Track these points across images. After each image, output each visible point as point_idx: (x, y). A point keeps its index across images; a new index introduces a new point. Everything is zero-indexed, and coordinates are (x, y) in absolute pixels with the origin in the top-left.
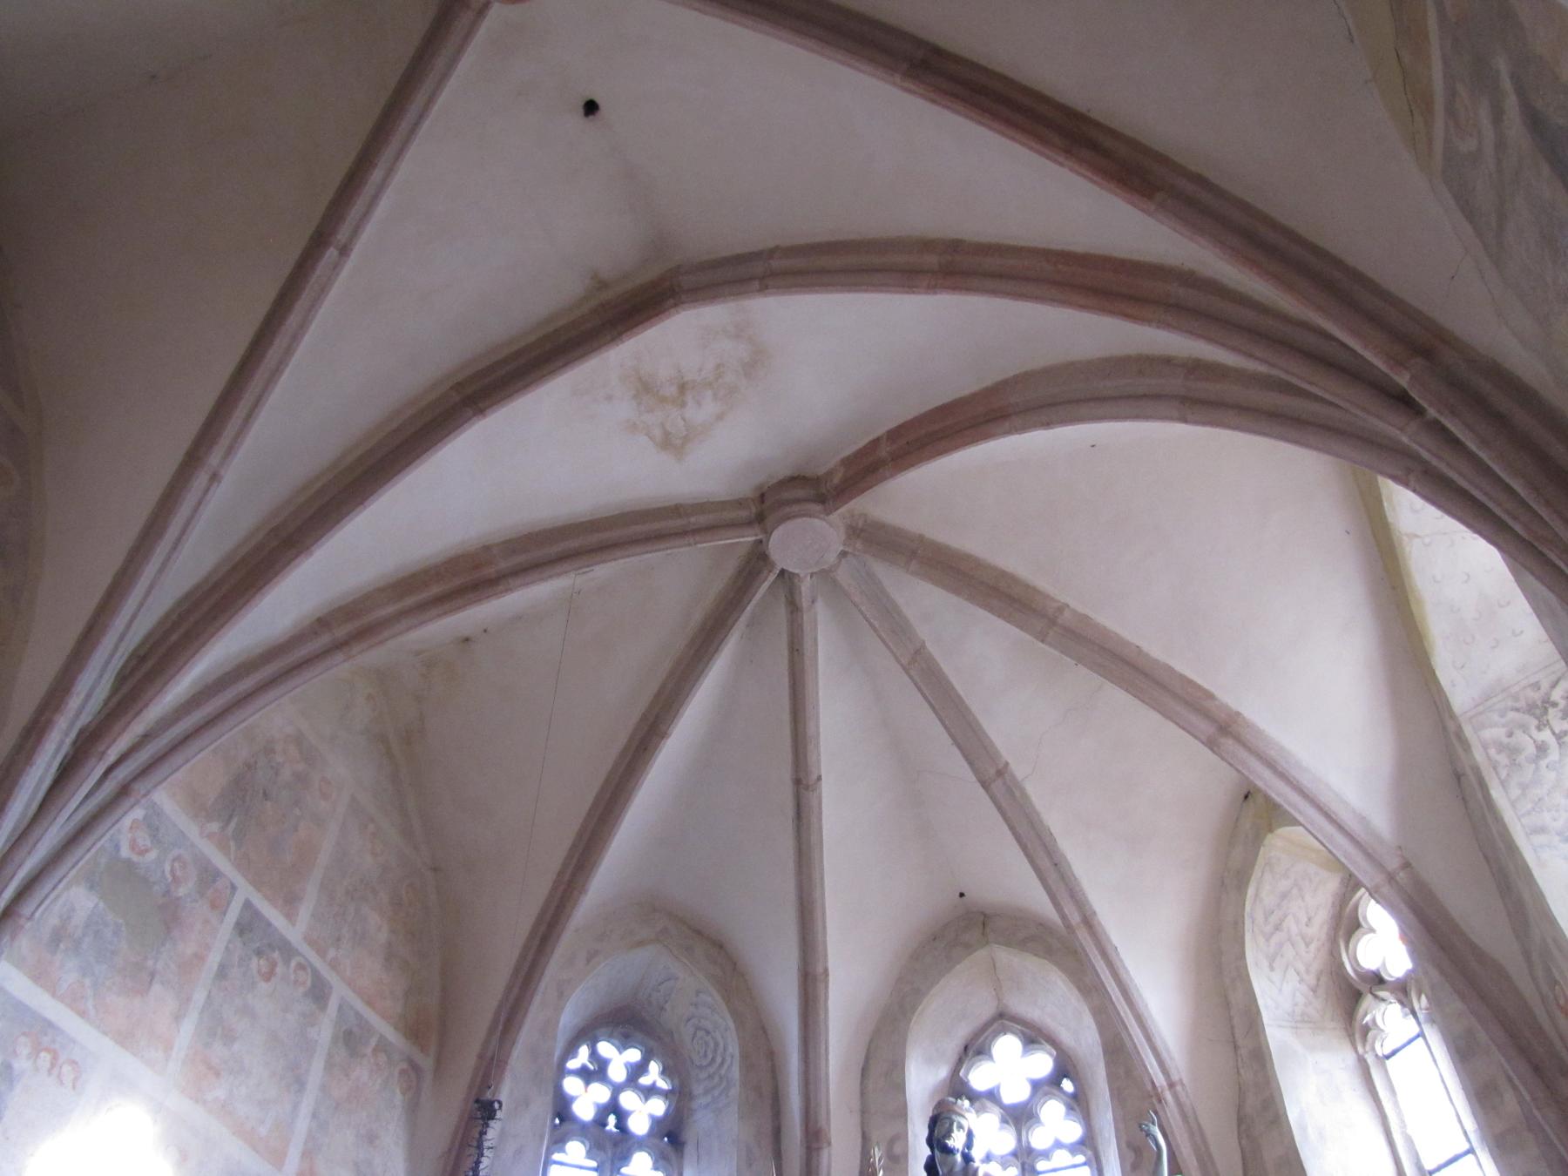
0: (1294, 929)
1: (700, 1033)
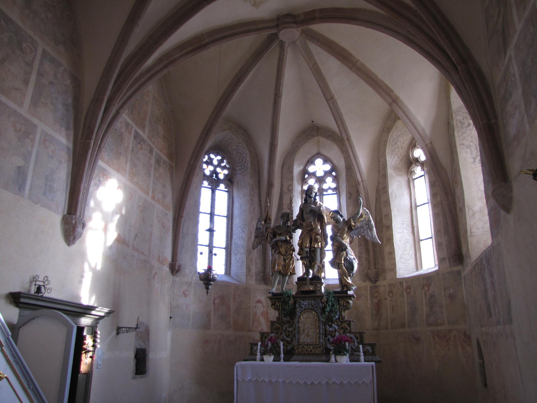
0: (399, 144)
1: (238, 154)
